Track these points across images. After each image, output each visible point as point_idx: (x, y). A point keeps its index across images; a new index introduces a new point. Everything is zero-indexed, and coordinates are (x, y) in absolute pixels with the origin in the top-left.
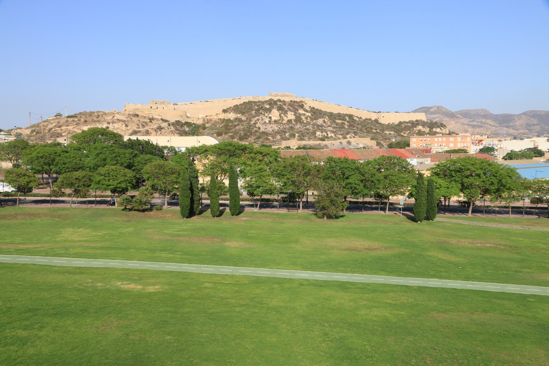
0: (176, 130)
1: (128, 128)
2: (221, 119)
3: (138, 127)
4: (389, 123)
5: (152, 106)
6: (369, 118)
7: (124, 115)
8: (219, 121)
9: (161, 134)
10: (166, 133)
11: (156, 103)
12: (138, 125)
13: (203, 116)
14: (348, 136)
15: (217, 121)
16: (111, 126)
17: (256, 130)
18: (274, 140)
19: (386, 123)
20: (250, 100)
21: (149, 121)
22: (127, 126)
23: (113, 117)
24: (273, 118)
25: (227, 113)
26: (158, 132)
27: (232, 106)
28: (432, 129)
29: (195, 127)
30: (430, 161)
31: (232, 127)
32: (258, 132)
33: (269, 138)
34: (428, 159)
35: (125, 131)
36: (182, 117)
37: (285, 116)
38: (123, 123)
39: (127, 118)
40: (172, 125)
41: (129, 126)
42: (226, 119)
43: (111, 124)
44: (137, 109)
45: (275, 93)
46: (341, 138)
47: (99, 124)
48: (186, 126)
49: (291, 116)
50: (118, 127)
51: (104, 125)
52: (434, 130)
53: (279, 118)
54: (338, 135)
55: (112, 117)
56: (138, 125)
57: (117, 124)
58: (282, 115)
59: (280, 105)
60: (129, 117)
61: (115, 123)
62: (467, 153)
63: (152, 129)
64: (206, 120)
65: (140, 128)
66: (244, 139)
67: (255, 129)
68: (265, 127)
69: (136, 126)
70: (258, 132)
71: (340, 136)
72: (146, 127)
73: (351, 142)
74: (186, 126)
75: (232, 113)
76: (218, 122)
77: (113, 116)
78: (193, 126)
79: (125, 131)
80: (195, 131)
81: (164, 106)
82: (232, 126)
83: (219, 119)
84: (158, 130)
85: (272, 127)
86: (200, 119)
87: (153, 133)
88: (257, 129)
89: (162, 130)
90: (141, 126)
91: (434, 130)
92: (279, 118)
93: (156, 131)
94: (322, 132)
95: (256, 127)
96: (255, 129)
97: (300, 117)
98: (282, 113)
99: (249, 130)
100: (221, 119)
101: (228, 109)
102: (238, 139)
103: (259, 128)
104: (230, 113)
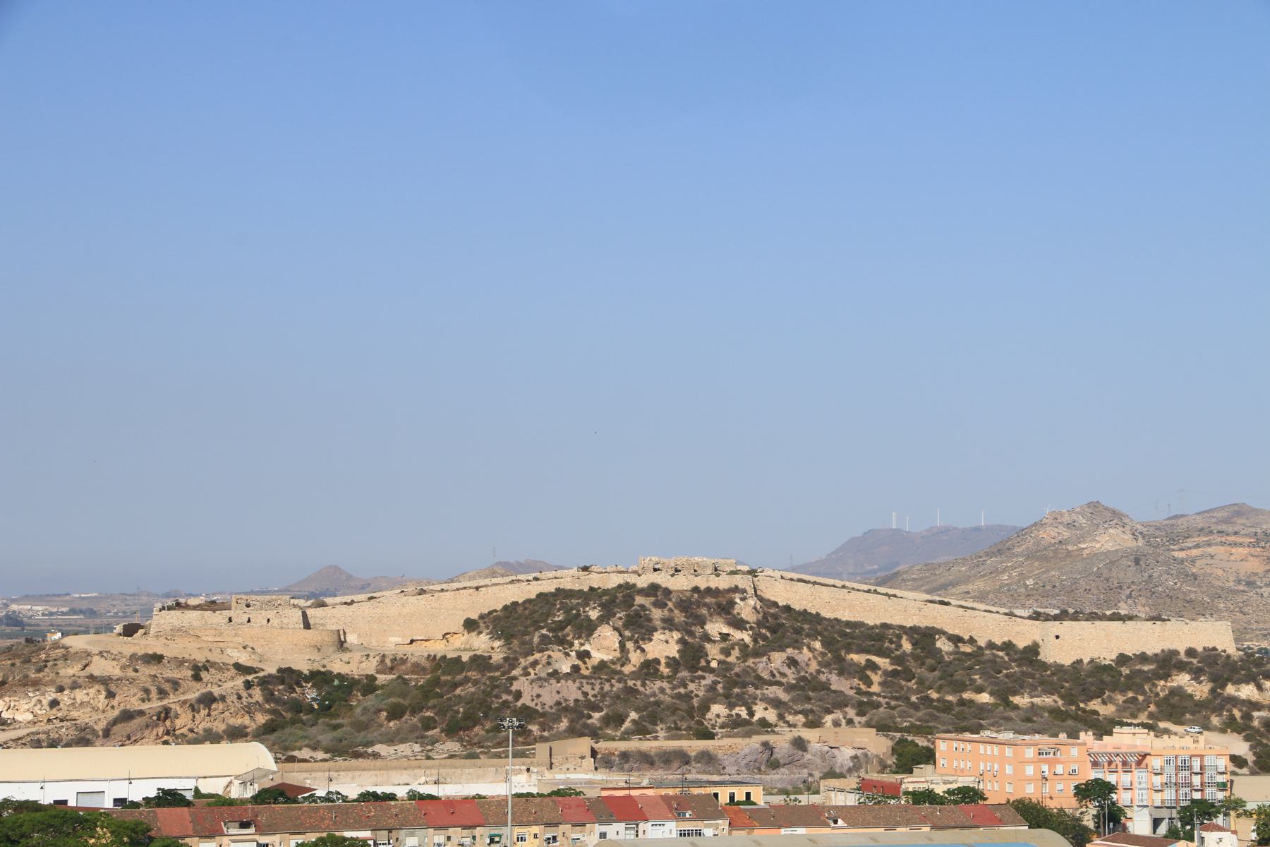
0: (267, 701)
1: (115, 702)
2: (435, 656)
3: (145, 696)
4: (1080, 662)
7: (118, 660)
9: (209, 715)
10: (227, 714)
11: (248, 606)
12: (147, 691)
13: (399, 640)
14: (828, 719)
15: (424, 663)
16: (66, 699)
17: (506, 702)
18: (546, 734)
19: (1067, 661)
20: (562, 587)
22: (111, 695)
23: (85, 666)
24: (597, 656)
26: (199, 712)
27: (499, 607)
28: (1223, 687)
30: (727, 827)
32: (509, 707)
33: (530, 727)
34: (720, 822)
35: (104, 712)
36: (319, 650)
37: (639, 648)
38: (102, 688)
39: (123, 668)
40: (258, 685)
41: (117, 698)
43: (66, 692)
44: (179, 630)
45: (655, 559)
46: (800, 724)
47: (34, 692)
48: (309, 685)
49: (663, 646)
50: (86, 699)
51: (47, 696)
52: (1230, 689)
53: (618, 654)
54: (790, 713)
55: (80, 666)
56: (147, 691)
57: (85, 692)
58: (630, 645)
59: (642, 606)
60: (129, 666)
61: (80, 687)
62: (986, 799)
63: (184, 702)
65: (149, 700)
66: (461, 729)
67: (505, 697)
68: (537, 690)
69: (140, 695)
70: (509, 707)
71: (801, 719)
72: (172, 696)
73: (809, 742)
74: (309, 685)
77: (84, 662)
78: (336, 682)
79: (104, 712)
80: (333, 701)
81: (271, 614)
83: (429, 656)
84: (202, 706)
85: (558, 692)
86: (371, 658)
87: (183, 716)
88: (510, 698)
89: (214, 706)
90: (154, 694)
91: (1230, 689)
92: (618, 654)
93: (193, 710)
94: (731, 706)
95: (509, 692)
96: (505, 697)
97: (703, 647)
98: (630, 639)
99: (485, 701)
100: (435, 656)
102: (442, 732)
103: (518, 695)
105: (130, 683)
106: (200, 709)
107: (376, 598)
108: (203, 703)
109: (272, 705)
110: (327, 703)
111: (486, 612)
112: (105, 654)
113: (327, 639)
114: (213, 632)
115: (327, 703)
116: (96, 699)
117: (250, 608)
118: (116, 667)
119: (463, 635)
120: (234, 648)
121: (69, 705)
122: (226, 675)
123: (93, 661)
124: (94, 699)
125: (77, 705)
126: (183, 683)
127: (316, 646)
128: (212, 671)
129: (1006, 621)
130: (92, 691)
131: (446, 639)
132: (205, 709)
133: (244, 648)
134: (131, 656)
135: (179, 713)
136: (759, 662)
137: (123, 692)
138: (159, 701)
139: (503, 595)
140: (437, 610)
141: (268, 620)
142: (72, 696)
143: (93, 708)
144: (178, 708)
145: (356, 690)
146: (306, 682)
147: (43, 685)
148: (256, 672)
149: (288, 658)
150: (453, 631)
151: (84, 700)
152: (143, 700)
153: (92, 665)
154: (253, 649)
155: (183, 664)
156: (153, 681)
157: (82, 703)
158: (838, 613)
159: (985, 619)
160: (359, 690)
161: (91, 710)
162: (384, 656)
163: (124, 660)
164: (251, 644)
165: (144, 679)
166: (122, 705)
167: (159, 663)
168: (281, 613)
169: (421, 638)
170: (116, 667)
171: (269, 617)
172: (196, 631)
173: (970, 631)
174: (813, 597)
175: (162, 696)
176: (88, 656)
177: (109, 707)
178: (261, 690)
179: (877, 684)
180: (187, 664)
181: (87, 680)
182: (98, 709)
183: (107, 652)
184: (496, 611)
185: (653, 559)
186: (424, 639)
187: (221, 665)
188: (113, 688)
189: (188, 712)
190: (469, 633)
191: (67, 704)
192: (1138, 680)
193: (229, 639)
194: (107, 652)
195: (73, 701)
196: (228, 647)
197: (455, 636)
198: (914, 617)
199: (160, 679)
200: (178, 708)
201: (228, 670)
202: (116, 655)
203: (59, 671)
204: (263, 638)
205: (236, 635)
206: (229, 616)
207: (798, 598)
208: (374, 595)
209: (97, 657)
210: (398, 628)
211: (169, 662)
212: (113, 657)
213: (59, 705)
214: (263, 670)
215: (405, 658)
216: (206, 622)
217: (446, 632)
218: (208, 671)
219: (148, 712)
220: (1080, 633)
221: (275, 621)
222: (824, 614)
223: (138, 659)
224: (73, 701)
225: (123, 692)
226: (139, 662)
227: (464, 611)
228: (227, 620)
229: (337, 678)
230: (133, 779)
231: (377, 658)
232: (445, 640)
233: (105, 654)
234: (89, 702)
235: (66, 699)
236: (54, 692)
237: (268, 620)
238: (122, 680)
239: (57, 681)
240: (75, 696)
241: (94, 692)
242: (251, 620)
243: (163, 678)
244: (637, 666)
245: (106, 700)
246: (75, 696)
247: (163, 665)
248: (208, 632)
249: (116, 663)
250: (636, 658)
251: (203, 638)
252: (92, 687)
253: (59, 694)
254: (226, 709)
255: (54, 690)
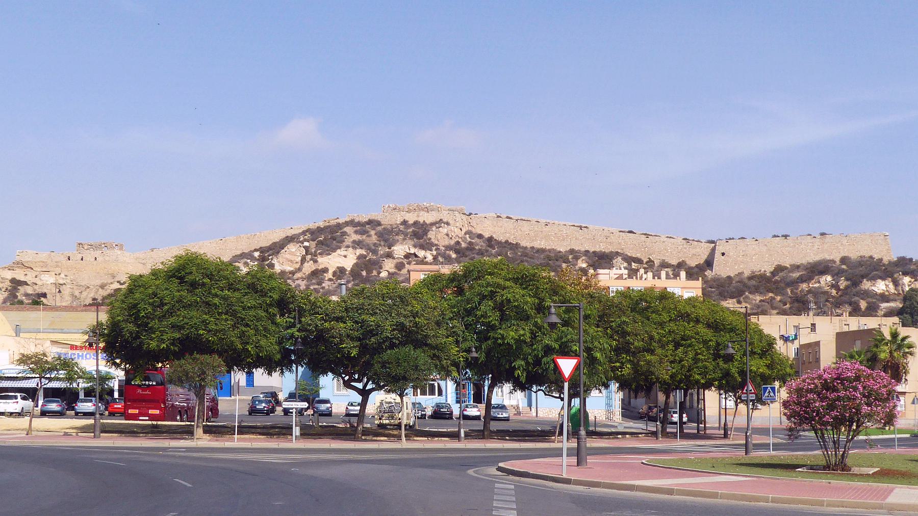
129: (683, 245)
136: (509, 280)
158: (535, 243)
159: (664, 244)
168: (104, 253)
173: (651, 255)
174: (516, 230)
179: (407, 270)
185: (391, 205)
192: (783, 285)
198: (601, 244)
204: (75, 268)
207: (502, 231)
220: (744, 249)
222: (524, 243)
230: (726, 410)
244: (307, 273)
250: (309, 267)
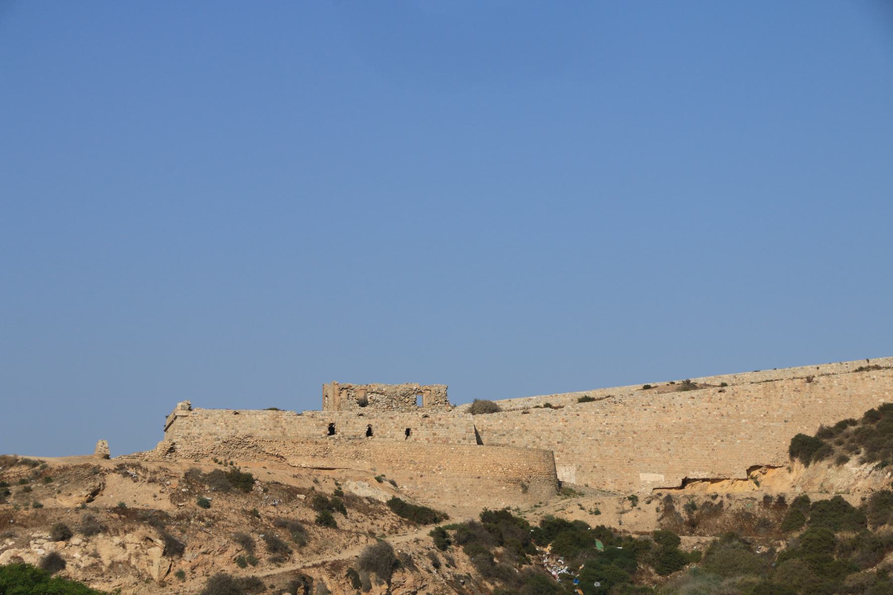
1: (184, 564)
3: (244, 553)
5: (335, 417)
6: (790, 441)
7: (162, 483)
8: (771, 516)
11: (363, 403)
15: (758, 511)
16: (77, 555)
21: (312, 515)
22: (174, 549)
23: (95, 493)
25: (820, 458)
27: (859, 415)
29: (610, 555)
31: (856, 555)
35: (162, 584)
36: (525, 489)
38: (153, 533)
39: (175, 497)
40: (460, 542)
41: (188, 555)
42: (815, 498)
43: (76, 540)
44: (241, 443)
48: (548, 549)
50: (121, 556)
51: (34, 547)
56: (247, 543)
57: (117, 540)
60: (189, 494)
61: (105, 530)
63: (336, 567)
64: (679, 508)
65: (255, 562)
69: (234, 550)
72: (296, 555)
74: (548, 549)
75: (854, 459)
76: (765, 524)
78: (599, 546)
81: (412, 419)
82: (854, 545)
84: (373, 576)
86: (641, 504)
89: (396, 577)
101: (825, 433)
104: (843, 460)
105: (208, 526)
106: (369, 582)
107: (592, 400)
108: (375, 570)
109: (498, 584)
110: (597, 584)
111: (832, 423)
112: (131, 471)
113: (537, 467)
114: (312, 448)
115: (597, 584)
116: (143, 557)
117: (367, 408)
118: (159, 496)
119: (790, 470)
120: (361, 479)
121: (85, 569)
122: (382, 524)
123: (108, 483)
124: (137, 555)
125: (104, 569)
126: (312, 531)
127: (519, 480)
128: (354, 514)
130: (133, 539)
131: (752, 478)
132: (381, 584)
133: (379, 480)
134: (186, 475)
135: (329, 587)
137: (197, 543)
138: (273, 566)
139: (862, 392)
140: (732, 421)
141: (408, 432)
142: (90, 548)
143: (140, 576)
144: (325, 578)
145: (645, 562)
146: (539, 544)
147: (21, 525)
148: (436, 521)
149: (466, 504)
150: (767, 463)
151: (117, 559)
152: (242, 563)
153: (105, 492)
154: (393, 483)
155: (295, 497)
156: (254, 523)
157: (113, 565)
160: (650, 563)
161: (136, 580)
162: (669, 498)
163: (175, 482)
164: (389, 476)
165: (235, 519)
166: (199, 571)
167: (247, 492)
168: (432, 417)
169: (705, 477)
170: (159, 496)
171: (410, 424)
172: (276, 446)
175: (277, 555)
176: (96, 473)
177: (172, 574)
178: (466, 552)
180: (302, 497)
181: (116, 516)
182: (150, 580)
183: (134, 466)
184: (853, 422)
186: (710, 477)
187: (366, 502)
188: (174, 530)
189: (347, 587)
190: (807, 465)
191: (83, 565)
193: (343, 464)
194: (134, 466)
195: (92, 560)
196: (347, 477)
197: (771, 472)
199: (265, 521)
200: (325, 578)
201: (382, 513)
202: (155, 473)
203: (41, 502)
205: (358, 455)
206: (329, 420)
208: (591, 394)
209: (114, 475)
210: (657, 455)
211: (265, 491)
212: (148, 476)
213: (64, 567)
214: (327, 562)
215: (716, 502)
216: (284, 434)
217: (752, 464)
218: (345, 513)
219: (267, 583)
221: (421, 434)
223: (203, 481)
224: (92, 560)
225: (197, 543)
226: (207, 487)
227: (786, 421)
228: (325, 429)
229: (599, 537)
231: (655, 504)
232: (751, 482)
233: (131, 471)
234: (128, 563)
235: (77, 555)
236: (49, 540)
237: (408, 432)
238: (189, 520)
239: (49, 518)
240: (95, 550)
241: (136, 540)
242: (375, 432)
243: (270, 519)
245: (164, 559)
246: (95, 550)
247: (257, 495)
248: (301, 449)
249: (160, 488)
251: (290, 461)
252: (132, 529)
253: (61, 544)
254: (419, 585)
255: (46, 535)
